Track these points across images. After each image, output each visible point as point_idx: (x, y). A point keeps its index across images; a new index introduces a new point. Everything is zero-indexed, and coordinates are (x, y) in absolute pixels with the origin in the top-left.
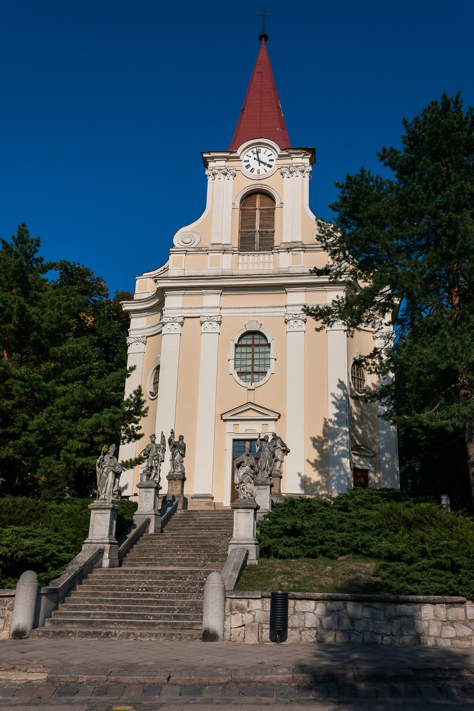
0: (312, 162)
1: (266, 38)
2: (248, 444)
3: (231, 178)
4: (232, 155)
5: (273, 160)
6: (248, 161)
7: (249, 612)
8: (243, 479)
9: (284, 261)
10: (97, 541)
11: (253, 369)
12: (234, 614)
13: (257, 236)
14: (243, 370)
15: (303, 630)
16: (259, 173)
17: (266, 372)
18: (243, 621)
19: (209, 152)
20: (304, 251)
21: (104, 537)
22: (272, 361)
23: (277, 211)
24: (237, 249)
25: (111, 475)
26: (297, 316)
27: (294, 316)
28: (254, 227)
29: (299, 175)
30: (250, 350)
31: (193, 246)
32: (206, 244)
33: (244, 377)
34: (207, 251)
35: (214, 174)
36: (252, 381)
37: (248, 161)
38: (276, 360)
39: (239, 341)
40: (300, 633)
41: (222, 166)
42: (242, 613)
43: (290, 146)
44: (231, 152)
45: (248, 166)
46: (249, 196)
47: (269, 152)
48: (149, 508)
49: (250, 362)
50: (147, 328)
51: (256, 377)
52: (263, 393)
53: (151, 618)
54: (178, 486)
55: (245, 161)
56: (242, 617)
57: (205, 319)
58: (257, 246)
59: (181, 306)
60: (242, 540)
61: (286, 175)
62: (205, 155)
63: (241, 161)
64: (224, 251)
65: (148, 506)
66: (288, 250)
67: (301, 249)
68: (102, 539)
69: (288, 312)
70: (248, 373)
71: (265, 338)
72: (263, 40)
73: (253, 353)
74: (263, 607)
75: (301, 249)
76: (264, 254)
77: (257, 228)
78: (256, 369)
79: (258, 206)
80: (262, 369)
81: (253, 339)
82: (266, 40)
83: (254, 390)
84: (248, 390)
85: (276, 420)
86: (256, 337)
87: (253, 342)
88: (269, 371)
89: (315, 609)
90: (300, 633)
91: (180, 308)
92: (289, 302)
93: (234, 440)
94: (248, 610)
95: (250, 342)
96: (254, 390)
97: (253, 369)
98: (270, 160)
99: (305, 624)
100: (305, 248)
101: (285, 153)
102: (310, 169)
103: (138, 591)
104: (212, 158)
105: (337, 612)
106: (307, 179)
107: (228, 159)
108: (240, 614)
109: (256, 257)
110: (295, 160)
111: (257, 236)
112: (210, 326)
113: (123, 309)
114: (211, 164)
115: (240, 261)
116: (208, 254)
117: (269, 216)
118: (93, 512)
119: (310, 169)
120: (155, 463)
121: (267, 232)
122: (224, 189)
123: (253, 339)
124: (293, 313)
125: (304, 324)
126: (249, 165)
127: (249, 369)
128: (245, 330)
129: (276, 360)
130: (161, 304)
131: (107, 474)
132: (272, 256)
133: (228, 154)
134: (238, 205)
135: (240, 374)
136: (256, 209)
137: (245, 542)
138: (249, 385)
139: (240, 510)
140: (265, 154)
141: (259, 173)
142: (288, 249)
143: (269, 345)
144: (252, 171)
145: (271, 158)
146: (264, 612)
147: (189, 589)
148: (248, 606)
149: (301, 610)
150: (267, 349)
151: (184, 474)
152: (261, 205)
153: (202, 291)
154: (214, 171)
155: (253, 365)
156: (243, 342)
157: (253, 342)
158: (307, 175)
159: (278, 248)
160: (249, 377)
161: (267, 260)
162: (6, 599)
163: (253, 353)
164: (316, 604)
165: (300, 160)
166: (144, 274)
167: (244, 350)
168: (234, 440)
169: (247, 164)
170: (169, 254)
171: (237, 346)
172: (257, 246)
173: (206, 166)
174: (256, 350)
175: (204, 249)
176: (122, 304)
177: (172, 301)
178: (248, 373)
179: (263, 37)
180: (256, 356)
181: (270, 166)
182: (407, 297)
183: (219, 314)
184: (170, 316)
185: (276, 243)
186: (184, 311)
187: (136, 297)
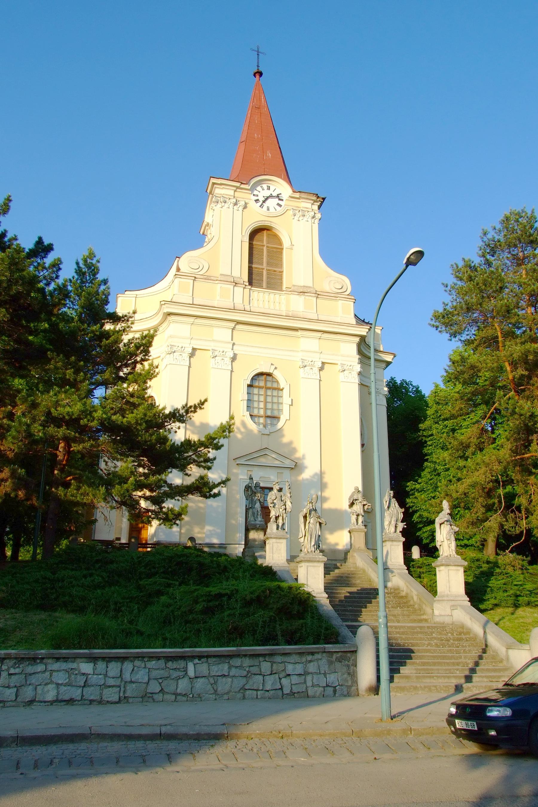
1: (261, 74)
4: (242, 186)
9: (298, 305)
13: (265, 273)
31: (201, 273)
41: (231, 196)
47: (265, 186)
53: (458, 672)
67: (314, 295)
79: (265, 243)
81: (266, 381)
87: (266, 384)
101: (297, 195)
106: (316, 227)
117: (276, 254)
118: (437, 569)
121: (275, 271)
122: (227, 218)
133: (238, 184)
136: (264, 246)
141: (268, 209)
147: (453, 644)
152: (268, 243)
157: (266, 384)
158: (317, 221)
162: (349, 655)
166: (126, 293)
169: (256, 198)
174: (269, 392)
175: (212, 278)
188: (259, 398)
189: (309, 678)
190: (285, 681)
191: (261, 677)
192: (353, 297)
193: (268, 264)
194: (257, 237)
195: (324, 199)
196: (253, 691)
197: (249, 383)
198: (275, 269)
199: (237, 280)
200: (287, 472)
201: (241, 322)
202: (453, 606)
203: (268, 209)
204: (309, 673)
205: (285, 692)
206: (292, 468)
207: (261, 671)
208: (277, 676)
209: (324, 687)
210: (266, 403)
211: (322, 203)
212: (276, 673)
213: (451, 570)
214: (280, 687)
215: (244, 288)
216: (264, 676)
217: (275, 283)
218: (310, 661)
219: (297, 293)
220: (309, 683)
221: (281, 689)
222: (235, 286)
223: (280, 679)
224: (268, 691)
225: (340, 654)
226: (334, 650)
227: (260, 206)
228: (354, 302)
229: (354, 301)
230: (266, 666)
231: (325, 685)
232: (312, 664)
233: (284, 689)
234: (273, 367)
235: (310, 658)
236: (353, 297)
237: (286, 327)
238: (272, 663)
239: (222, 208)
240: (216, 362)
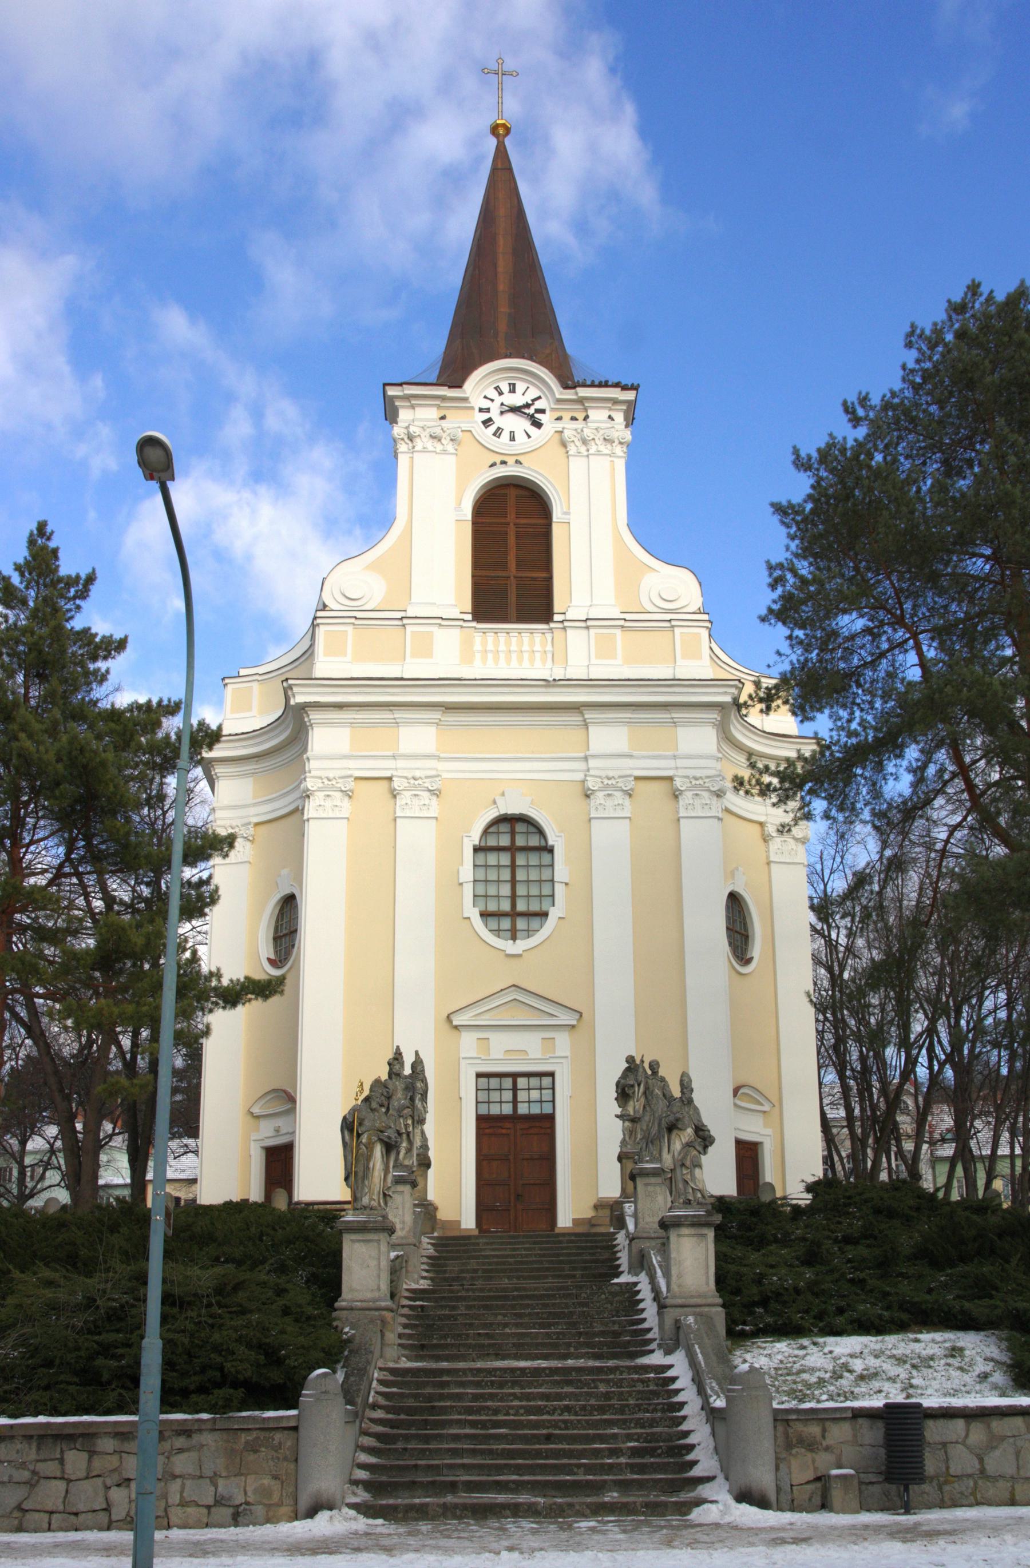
0: (630, 420)
2: (508, 1083)
6: (488, 410)
7: (827, 1449)
8: (684, 1158)
10: (364, 1305)
12: (795, 1456)
14: (492, 907)
15: (946, 1482)
17: (545, 915)
18: (816, 1469)
21: (376, 1295)
22: (559, 889)
25: (378, 1150)
28: (505, 567)
30: (505, 859)
33: (493, 923)
37: (488, 410)
38: (566, 884)
40: (940, 1489)
42: (812, 1451)
45: (487, 423)
51: (521, 924)
55: (481, 410)
56: (814, 1461)
60: (692, 1297)
62: (391, 392)
63: (472, 408)
68: (375, 1300)
71: (541, 832)
74: (855, 1436)
78: (521, 907)
80: (535, 907)
81: (513, 833)
86: (520, 827)
88: (554, 913)
89: (967, 1436)
90: (940, 1489)
92: (404, 748)
93: (479, 1075)
94: (824, 1444)
95: (505, 841)
96: (520, 956)
99: (948, 1468)
103: (507, 1414)
104: (408, 398)
105: (1011, 1440)
106: (620, 465)
108: (809, 1455)
112: (416, 801)
115: (478, 646)
116: (587, 628)
118: (347, 1240)
119: (627, 435)
120: (406, 1126)
123: (513, 833)
124: (603, 774)
125: (627, 801)
126: (490, 420)
127: (506, 906)
128: (492, 814)
131: (370, 1147)
135: (484, 915)
137: (699, 1301)
139: (685, 1231)
141: (512, 438)
143: (551, 850)
144: (498, 433)
146: (860, 1449)
148: (824, 1437)
149: (937, 1438)
150: (546, 858)
153: (674, 715)
156: (492, 842)
158: (620, 451)
160: (506, 923)
164: (968, 1425)
168: (479, 1075)
177: (326, 739)
182: (949, 745)
189: (175, 1486)
190: (118, 1495)
191: (61, 1485)
192: (706, 617)
196: (42, 1514)
197: (477, 842)
200: (563, 1042)
201: (464, 706)
202: (120, 1319)
203: (512, 438)
204: (175, 1477)
205: (114, 1518)
206: (573, 1026)
207: (63, 1471)
208: (99, 1481)
209: (209, 1507)
210: (513, 882)
212: (99, 1476)
213: (684, 1235)
214: (104, 1506)
216: (69, 1481)
218: (181, 1450)
220: (175, 1498)
221: (107, 1510)
223: (108, 1488)
224: (76, 1514)
225: (255, 1434)
226: (236, 1427)
227: (494, 434)
228: (710, 629)
229: (708, 625)
230: (76, 1460)
231: (210, 1501)
232: (186, 1455)
233: (114, 1511)
235: (180, 1442)
237: (464, 706)
238: (92, 1453)
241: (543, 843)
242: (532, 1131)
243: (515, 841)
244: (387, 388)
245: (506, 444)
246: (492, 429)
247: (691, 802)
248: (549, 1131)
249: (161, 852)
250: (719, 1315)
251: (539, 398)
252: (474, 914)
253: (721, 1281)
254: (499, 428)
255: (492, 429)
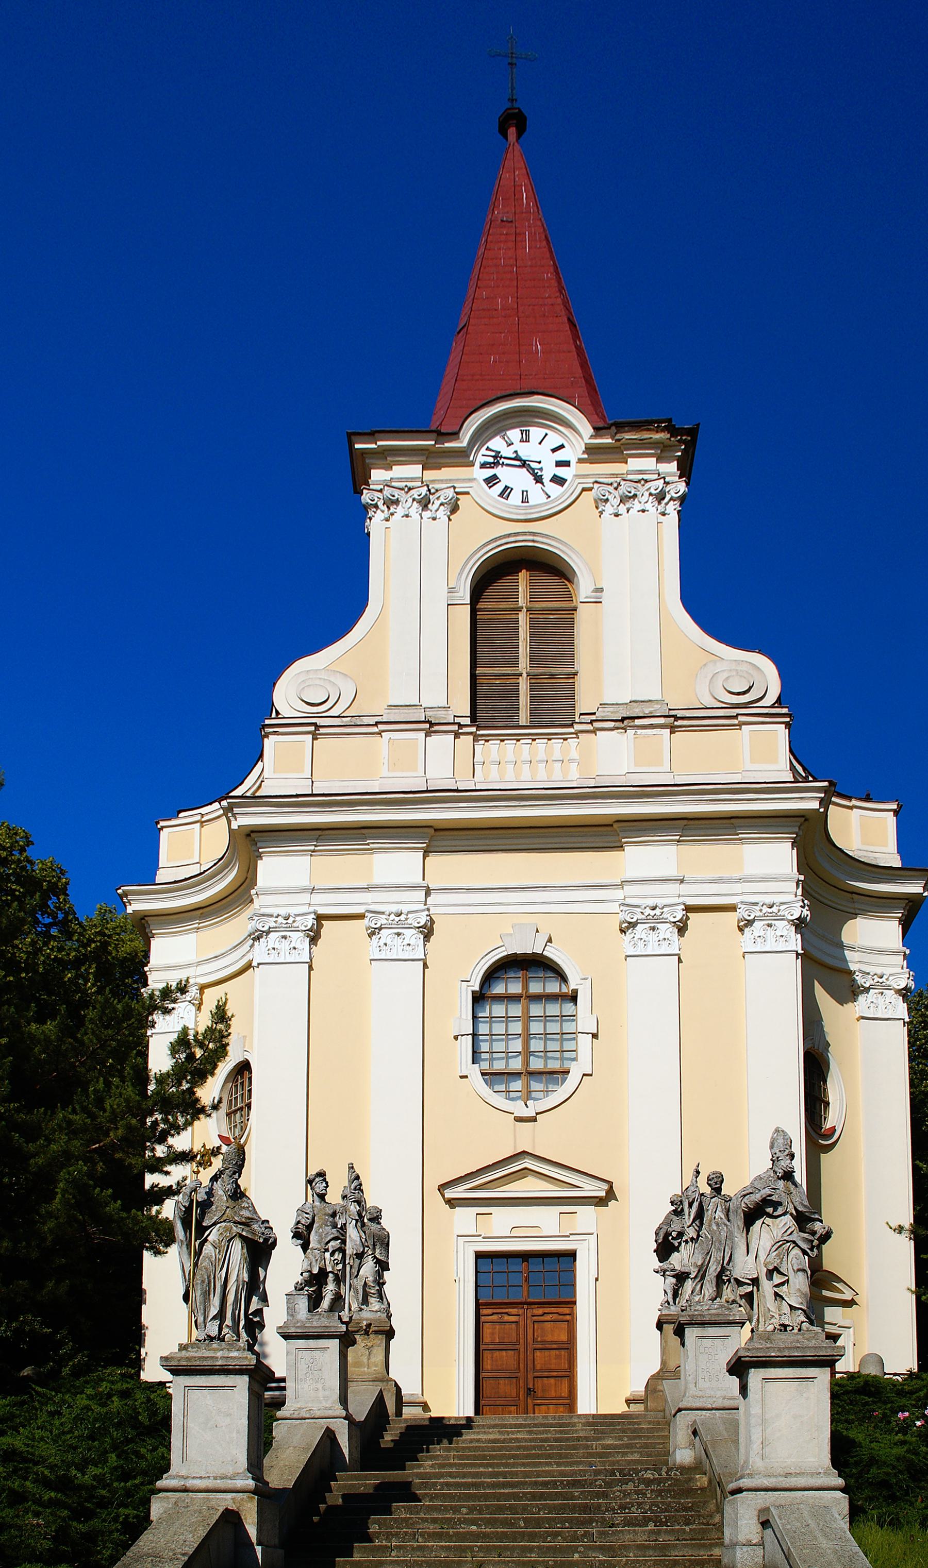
0: (685, 471)
3: (442, 513)
5: (566, 464)
9: (613, 758)
11: (526, 1063)
13: (524, 685)
16: (525, 500)
19: (372, 435)
20: (673, 729)
22: (584, 1041)
23: (584, 617)
24: (467, 721)
26: (658, 912)
27: (648, 911)
28: (515, 663)
29: (648, 506)
30: (516, 1010)
32: (374, 706)
34: (380, 726)
35: (391, 502)
36: (528, 1096)
38: (595, 1036)
39: (482, 985)
41: (413, 479)
43: (619, 422)
44: (441, 435)
46: (494, 573)
48: (326, 1398)
49: (517, 1045)
50: (199, 964)
51: (535, 1086)
52: (561, 1130)
54: (375, 1351)
57: (382, 920)
58: (524, 717)
59: (305, 883)
61: (609, 509)
64: (431, 727)
65: (321, 1394)
66: (625, 722)
67: (662, 721)
69: (628, 901)
70: (516, 1075)
71: (562, 977)
72: (512, 132)
73: (527, 1019)
75: (662, 721)
76: (549, 737)
77: (524, 664)
78: (536, 1064)
80: (554, 1065)
82: (520, 132)
83: (534, 1119)
84: (519, 1120)
85: (601, 1202)
91: (303, 890)
93: (479, 1256)
95: (515, 988)
96: (534, 1119)
97: (526, 1063)
98: (559, 464)
100: (676, 718)
102: (682, 487)
106: (672, 520)
107: (430, 460)
109: (524, 747)
110: (634, 464)
111: (524, 685)
112: (398, 941)
113: (130, 910)
114: (377, 475)
117: (557, 631)
121: (552, 676)
122: (419, 549)
129: (595, 1036)
130: (248, 880)
132: (573, 742)
134: (464, 594)
135: (490, 1077)
136: (519, 609)
138: (520, 1109)
140: (538, 445)
141: (525, 500)
142: (623, 720)
143: (573, 998)
144: (506, 492)
145: (561, 456)
150: (568, 1008)
151: (389, 1317)
152: (532, 598)
154: (387, 492)
155: (527, 1053)
158: (672, 509)
159: (593, 717)
160: (517, 1085)
161: (557, 755)
163: (527, 1019)
165: (649, 463)
166: (181, 815)
167: (499, 1010)
168: (479, 1256)
170: (260, 733)
171: (479, 998)
172: (524, 717)
173: (360, 480)
174: (536, 1010)
175: (366, 721)
176: (126, 894)
178: (516, 1075)
179: (513, 120)
180: (536, 1028)
181: (559, 481)
183: (422, 907)
184: (275, 911)
185: (585, 702)
186: (317, 898)
187: (162, 876)
188: (491, 1047)
193: (534, 659)
194: (494, 589)
195: (693, 432)
197: (477, 988)
198: (553, 671)
199: (434, 716)
200: (587, 1213)
210: (527, 1037)
211: (691, 447)
215: (457, 735)
217: (555, 708)
219: (612, 724)
222: (428, 734)
227: (501, 495)
234: (542, 939)
236: (785, 711)
239: (387, 520)
240: (381, 943)
241: (565, 990)
242: (548, 1317)
243: (522, 975)
244: (353, 437)
245: (517, 507)
246: (499, 488)
247: (762, 933)
248: (568, 1317)
249: (228, 1153)
250: (841, 1501)
251: (562, 447)
252: (474, 1071)
253: (842, 1451)
254: (506, 488)
255: (499, 488)
